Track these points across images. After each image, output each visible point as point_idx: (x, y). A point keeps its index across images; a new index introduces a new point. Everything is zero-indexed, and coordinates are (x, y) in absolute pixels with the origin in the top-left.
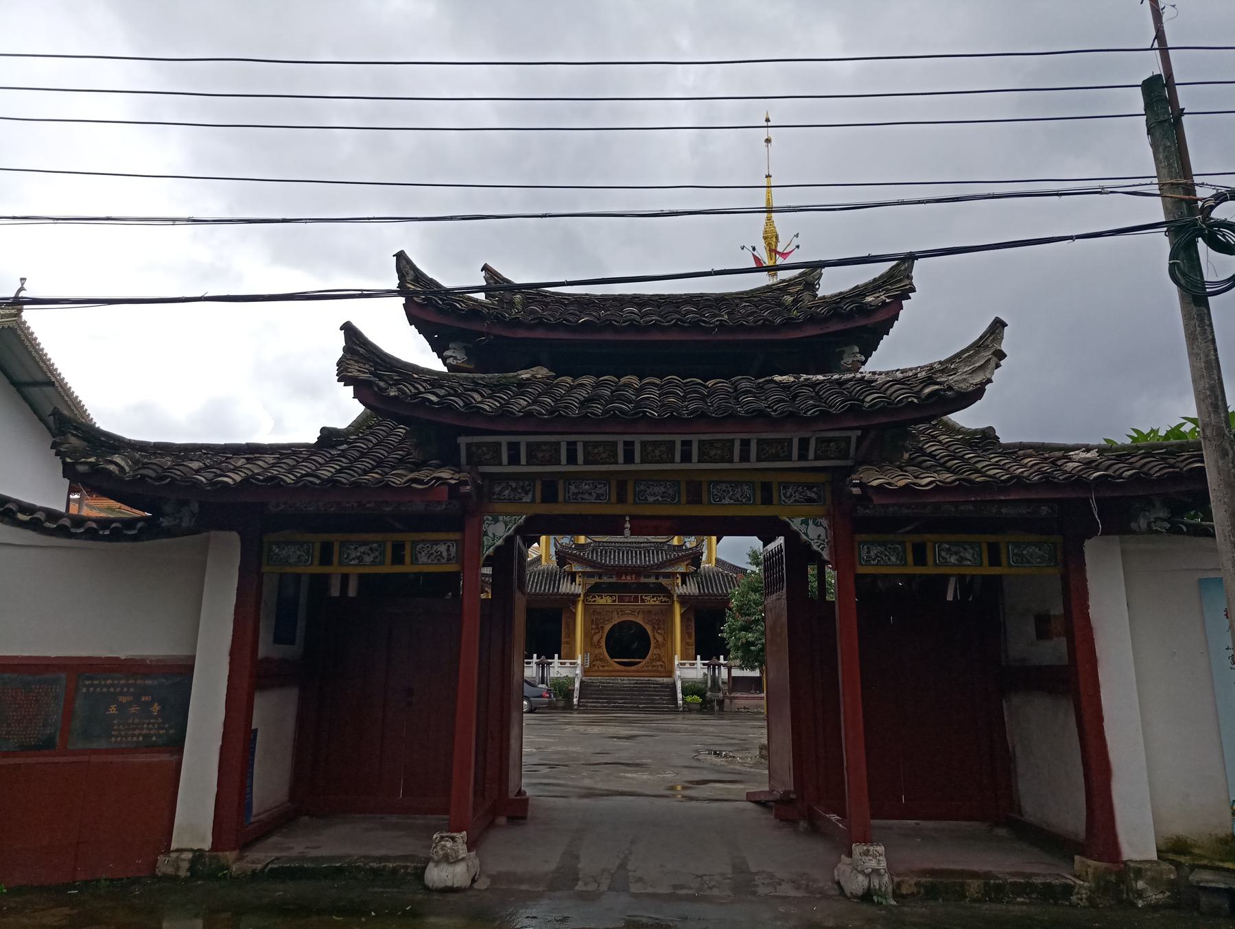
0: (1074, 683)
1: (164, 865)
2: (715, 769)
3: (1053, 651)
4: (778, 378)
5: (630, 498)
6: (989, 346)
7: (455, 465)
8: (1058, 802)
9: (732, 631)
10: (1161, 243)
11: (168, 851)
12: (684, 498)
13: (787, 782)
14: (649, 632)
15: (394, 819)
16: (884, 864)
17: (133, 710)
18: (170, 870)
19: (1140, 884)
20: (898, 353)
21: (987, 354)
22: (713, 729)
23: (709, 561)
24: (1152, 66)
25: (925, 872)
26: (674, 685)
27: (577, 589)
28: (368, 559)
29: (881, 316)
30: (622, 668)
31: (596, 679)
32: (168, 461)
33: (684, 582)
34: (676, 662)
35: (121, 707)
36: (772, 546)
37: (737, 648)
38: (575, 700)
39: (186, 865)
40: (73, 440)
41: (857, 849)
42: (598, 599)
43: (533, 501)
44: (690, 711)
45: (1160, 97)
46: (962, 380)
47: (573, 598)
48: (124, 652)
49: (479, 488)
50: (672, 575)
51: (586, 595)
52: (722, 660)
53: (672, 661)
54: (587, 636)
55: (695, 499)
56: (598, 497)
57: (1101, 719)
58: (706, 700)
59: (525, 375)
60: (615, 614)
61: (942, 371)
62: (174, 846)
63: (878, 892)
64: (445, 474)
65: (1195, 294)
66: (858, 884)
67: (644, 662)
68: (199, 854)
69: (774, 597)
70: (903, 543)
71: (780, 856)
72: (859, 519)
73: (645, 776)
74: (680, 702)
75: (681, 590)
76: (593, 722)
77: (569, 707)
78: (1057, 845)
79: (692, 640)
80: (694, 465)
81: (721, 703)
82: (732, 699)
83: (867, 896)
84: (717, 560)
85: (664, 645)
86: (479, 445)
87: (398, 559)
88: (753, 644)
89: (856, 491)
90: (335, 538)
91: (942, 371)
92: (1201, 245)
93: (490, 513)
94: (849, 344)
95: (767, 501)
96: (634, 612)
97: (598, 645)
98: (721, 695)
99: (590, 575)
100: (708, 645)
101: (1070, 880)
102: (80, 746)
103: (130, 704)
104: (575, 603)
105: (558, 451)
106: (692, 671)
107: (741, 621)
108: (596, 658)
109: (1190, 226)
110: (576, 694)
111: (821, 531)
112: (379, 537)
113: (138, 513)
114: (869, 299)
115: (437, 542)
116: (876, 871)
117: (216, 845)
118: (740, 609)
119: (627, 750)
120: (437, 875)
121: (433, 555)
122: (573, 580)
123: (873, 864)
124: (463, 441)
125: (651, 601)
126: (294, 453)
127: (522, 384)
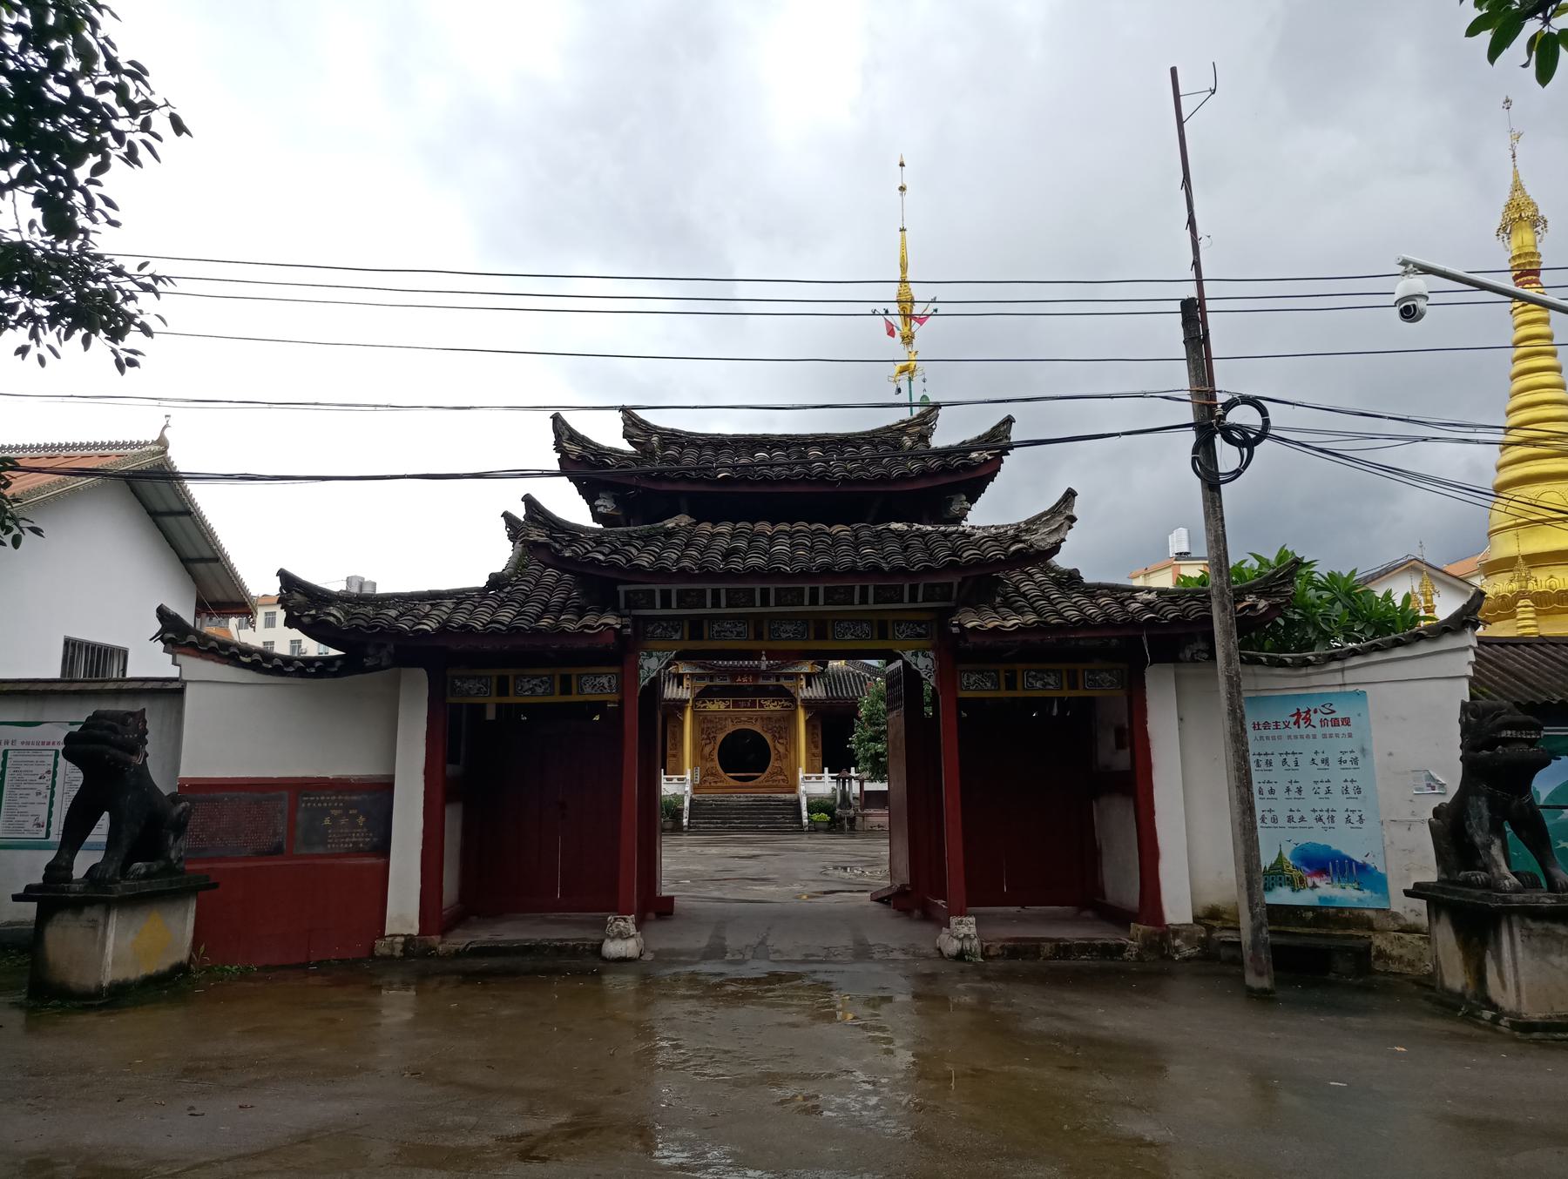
0: (1135, 785)
1: (381, 948)
2: (842, 881)
3: (1122, 760)
4: (894, 526)
5: (766, 636)
6: (1063, 510)
7: (616, 610)
8: (1123, 888)
9: (861, 742)
10: (1190, 437)
11: (382, 936)
12: (812, 636)
13: (904, 877)
15: (552, 916)
16: (974, 930)
17: (343, 822)
18: (387, 951)
19: (1178, 942)
20: (995, 510)
21: (1061, 519)
22: (842, 847)
24: (1190, 291)
25: (1010, 940)
26: (798, 803)
27: (684, 693)
28: (539, 690)
29: (983, 472)
30: (738, 783)
31: (709, 796)
32: (369, 610)
33: (809, 684)
34: (801, 776)
35: (333, 819)
36: (893, 666)
37: (866, 760)
38: (685, 821)
39: (400, 947)
40: (297, 596)
41: (954, 920)
42: (709, 704)
43: (682, 638)
44: (816, 830)
45: (1193, 313)
46: (1041, 539)
47: (680, 705)
48: (331, 773)
49: (635, 629)
51: (695, 700)
52: (853, 773)
54: (696, 746)
55: (821, 635)
56: (738, 634)
57: (1153, 813)
58: (836, 819)
59: (670, 524)
60: (729, 722)
61: (1027, 531)
62: (387, 932)
63: (970, 953)
64: (611, 620)
65: (1212, 482)
66: (953, 947)
67: (763, 776)
68: (409, 939)
69: (895, 713)
70: (997, 672)
71: (894, 934)
72: (960, 654)
73: (772, 888)
74: (805, 821)
75: (805, 693)
76: (708, 844)
77: (348, 958)
78: (1119, 917)
79: (819, 751)
80: (821, 608)
81: (852, 820)
82: (863, 816)
83: (960, 956)
86: (636, 592)
87: (566, 690)
88: (882, 755)
89: (955, 630)
90: (511, 673)
91: (1027, 531)
92: (1218, 439)
93: (645, 649)
94: (958, 492)
95: (883, 636)
96: (751, 718)
97: (709, 758)
98: (852, 812)
99: (700, 677)
100: (835, 758)
101: (1124, 940)
102: (304, 851)
103: (340, 816)
105: (704, 597)
106: (821, 785)
107: (870, 732)
108: (707, 773)
109: (1209, 426)
110: (686, 814)
111: (929, 662)
112: (548, 671)
113: (333, 652)
114: (974, 455)
115: (600, 675)
116: (966, 936)
117: (423, 931)
118: (869, 718)
119: (752, 868)
120: (613, 948)
121: (599, 686)
122: (680, 684)
123: (965, 930)
124: (621, 589)
125: (771, 706)
126: (468, 597)
127: (670, 534)
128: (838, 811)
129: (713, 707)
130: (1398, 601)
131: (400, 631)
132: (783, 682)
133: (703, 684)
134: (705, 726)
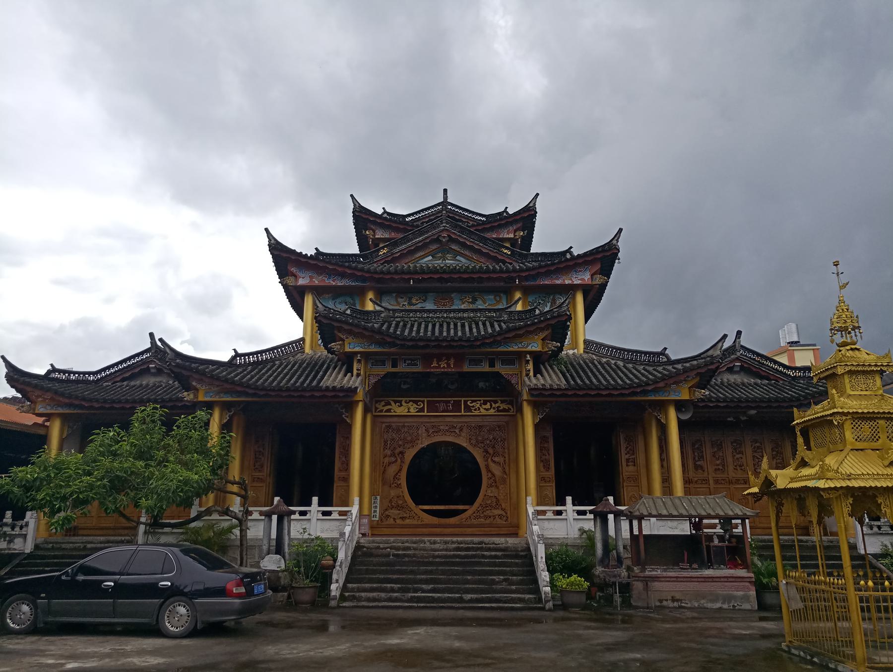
14: (480, 460)
23: (575, 346)
26: (526, 557)
30: (435, 520)
31: (388, 542)
33: (537, 371)
34: (530, 510)
42: (394, 406)
44: (564, 607)
53: (517, 507)
67: (471, 510)
79: (552, 472)
82: (647, 580)
84: (586, 342)
85: (504, 481)
96: (457, 426)
104: (350, 407)
108: (390, 505)
110: (339, 576)
122: (350, 370)
125: (484, 410)
128: (599, 570)
129: (401, 411)
130: (569, 507)
132: (499, 368)
133: (382, 371)
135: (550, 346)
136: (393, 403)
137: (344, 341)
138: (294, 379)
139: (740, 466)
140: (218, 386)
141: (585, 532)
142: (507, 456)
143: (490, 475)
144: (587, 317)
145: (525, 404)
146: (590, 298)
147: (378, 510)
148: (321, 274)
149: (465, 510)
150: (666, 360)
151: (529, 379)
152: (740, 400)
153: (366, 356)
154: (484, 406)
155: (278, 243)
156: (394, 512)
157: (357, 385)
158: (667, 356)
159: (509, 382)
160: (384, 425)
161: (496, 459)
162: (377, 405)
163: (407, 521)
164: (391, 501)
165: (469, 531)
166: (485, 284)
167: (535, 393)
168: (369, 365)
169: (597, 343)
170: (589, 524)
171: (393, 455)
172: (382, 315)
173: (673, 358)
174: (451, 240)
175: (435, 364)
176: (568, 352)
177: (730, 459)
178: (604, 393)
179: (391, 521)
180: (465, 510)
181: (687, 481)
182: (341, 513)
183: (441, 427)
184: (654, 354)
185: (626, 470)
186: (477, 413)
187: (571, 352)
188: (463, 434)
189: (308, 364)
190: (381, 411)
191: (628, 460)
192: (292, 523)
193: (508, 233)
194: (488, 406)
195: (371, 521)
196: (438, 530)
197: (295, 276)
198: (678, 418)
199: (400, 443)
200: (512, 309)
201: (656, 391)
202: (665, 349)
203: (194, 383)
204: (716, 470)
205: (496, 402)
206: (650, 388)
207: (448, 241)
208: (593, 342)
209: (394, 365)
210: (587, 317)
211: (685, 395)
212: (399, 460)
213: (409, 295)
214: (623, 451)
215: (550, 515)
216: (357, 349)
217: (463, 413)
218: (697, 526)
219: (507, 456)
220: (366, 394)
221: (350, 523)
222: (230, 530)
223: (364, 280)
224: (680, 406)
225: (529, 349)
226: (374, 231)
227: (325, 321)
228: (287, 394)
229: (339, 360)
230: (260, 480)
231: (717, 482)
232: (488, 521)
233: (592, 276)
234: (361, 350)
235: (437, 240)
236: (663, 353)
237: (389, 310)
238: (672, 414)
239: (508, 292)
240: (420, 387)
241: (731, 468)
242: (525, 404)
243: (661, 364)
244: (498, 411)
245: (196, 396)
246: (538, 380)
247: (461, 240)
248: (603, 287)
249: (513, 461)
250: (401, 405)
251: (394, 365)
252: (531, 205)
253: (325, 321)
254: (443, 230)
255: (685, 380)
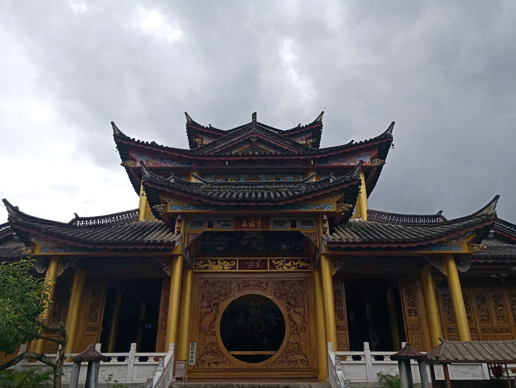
23: (360, 215)
30: (244, 365)
34: (332, 356)
42: (211, 264)
46: (439, 214)
50: (314, 218)
67: (276, 355)
85: (304, 329)
104: (171, 260)
125: (286, 267)
129: (217, 268)
130: (367, 352)
131: (60, 276)
133: (199, 230)
134: (206, 291)
135: (343, 207)
136: (210, 262)
137: (166, 203)
138: (121, 236)
139: (502, 317)
140: (53, 242)
141: (384, 377)
142: (306, 307)
143: (292, 324)
144: (368, 195)
145: (323, 258)
146: (370, 176)
147: (195, 355)
148: (155, 159)
149: (272, 355)
150: (442, 221)
151: (326, 236)
152: (505, 258)
153: (186, 217)
154: (286, 264)
155: (121, 133)
156: (208, 358)
157: (176, 239)
158: (443, 218)
159: (308, 240)
160: (202, 281)
161: (297, 310)
162: (197, 264)
163: (220, 366)
164: (206, 348)
165: (274, 374)
166: (287, 166)
167: (333, 246)
168: (189, 226)
169: (378, 213)
170: (393, 370)
171: (209, 306)
172: (202, 187)
173: (449, 219)
174: (259, 141)
175: (245, 225)
176: (354, 219)
177: (493, 312)
178: (394, 246)
179: (206, 366)
180: (272, 355)
181: (472, 330)
182: (156, 359)
183: (250, 282)
184: (431, 217)
185: (409, 320)
186: (280, 270)
187: (357, 220)
188: (269, 289)
189: (138, 228)
190: (200, 268)
191: (410, 311)
192: (101, 369)
193: (302, 141)
194: (289, 264)
195: (187, 366)
196: (247, 374)
197: (134, 160)
198: (458, 270)
199: (216, 296)
200: (310, 181)
201: (439, 245)
202: (441, 212)
203: (33, 240)
204: (482, 320)
205: (296, 261)
206: (435, 242)
207: (257, 141)
208: (374, 212)
209: (210, 226)
210: (368, 195)
211: (465, 250)
212: (214, 310)
213: (226, 176)
214: (406, 303)
215: (349, 360)
216: (178, 210)
217: (269, 270)
218: (497, 371)
219: (306, 307)
220: (185, 250)
221: (162, 369)
222: (46, 377)
223: (190, 162)
224: (459, 259)
225: (326, 210)
226: (202, 139)
227: (150, 186)
228: (113, 247)
229: (165, 225)
230: (94, 329)
231: (484, 331)
232: (291, 366)
233: (372, 159)
234: (181, 211)
235: (249, 141)
236: (439, 215)
237: (208, 183)
238: (453, 266)
239: (304, 173)
240: (234, 246)
241: (495, 319)
242: (323, 258)
243: (437, 224)
244: (298, 268)
245: (33, 251)
246: (334, 236)
247: (267, 140)
248: (380, 168)
249: (310, 312)
250: (217, 264)
251: (210, 226)
252: (318, 120)
253: (150, 186)
254: (253, 133)
255: (463, 236)
